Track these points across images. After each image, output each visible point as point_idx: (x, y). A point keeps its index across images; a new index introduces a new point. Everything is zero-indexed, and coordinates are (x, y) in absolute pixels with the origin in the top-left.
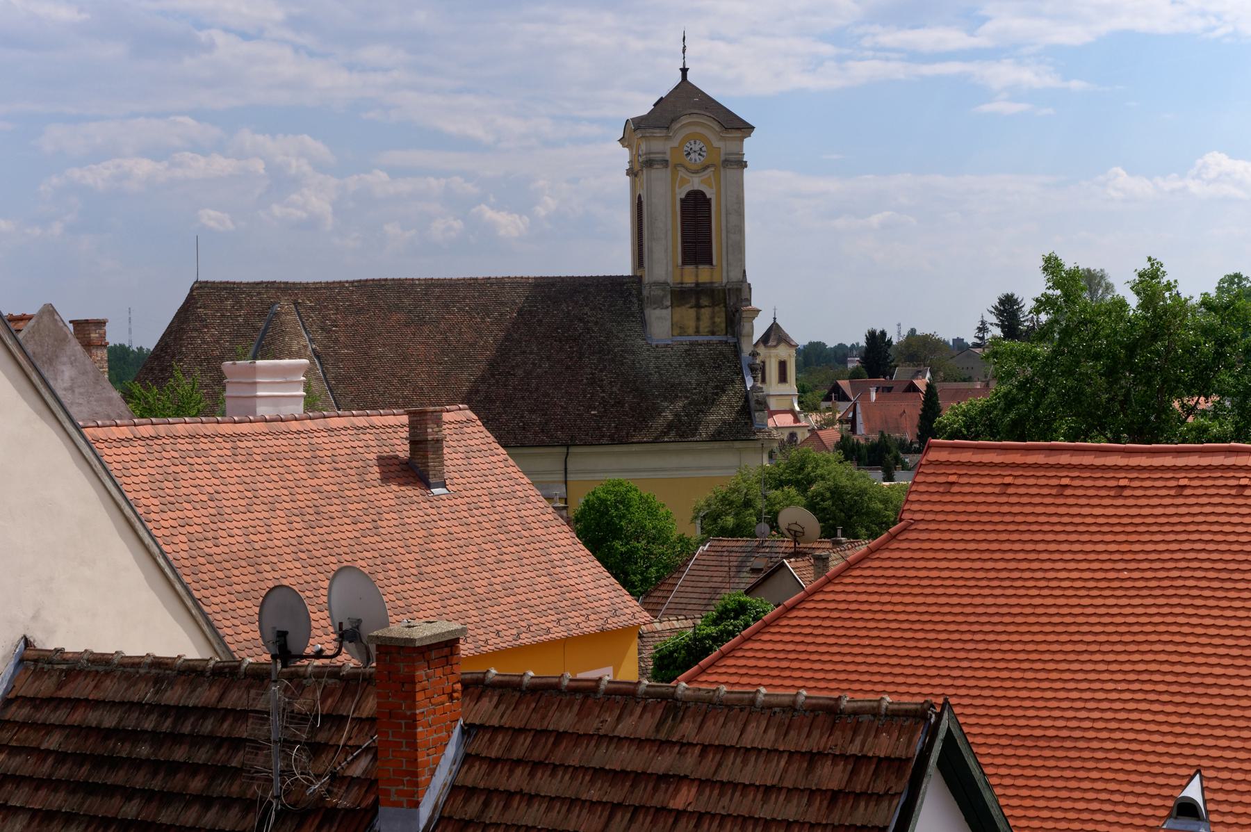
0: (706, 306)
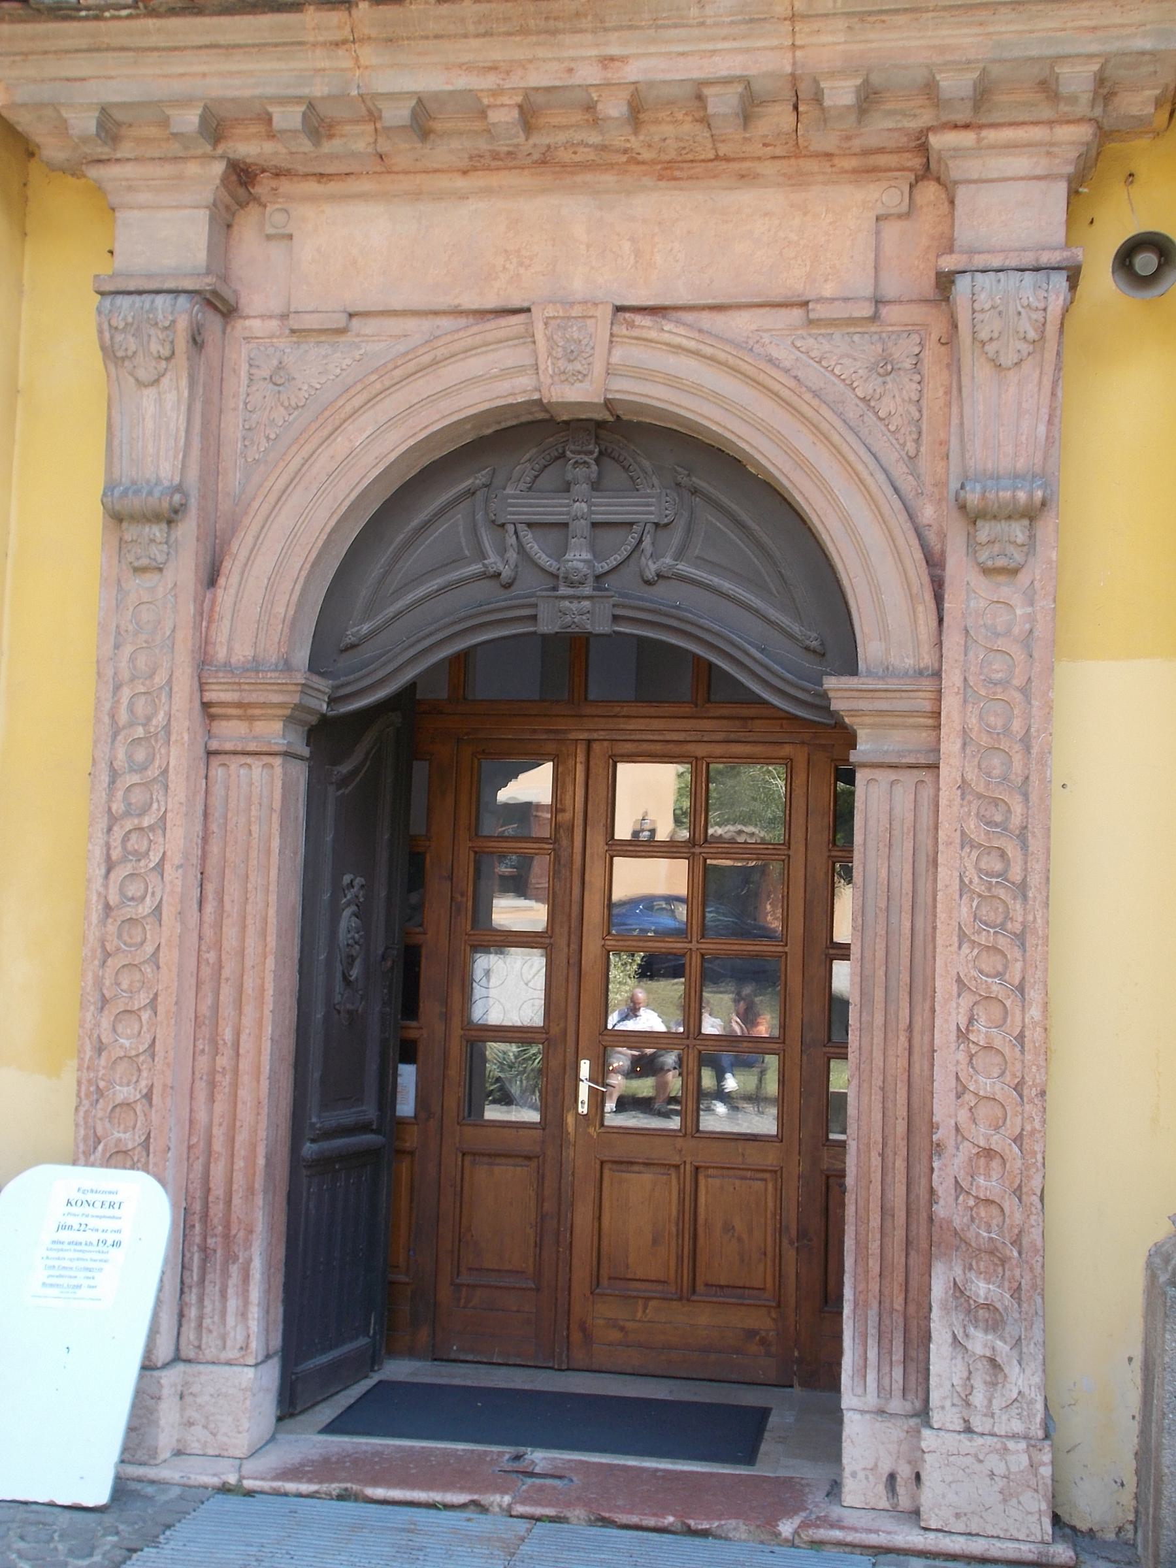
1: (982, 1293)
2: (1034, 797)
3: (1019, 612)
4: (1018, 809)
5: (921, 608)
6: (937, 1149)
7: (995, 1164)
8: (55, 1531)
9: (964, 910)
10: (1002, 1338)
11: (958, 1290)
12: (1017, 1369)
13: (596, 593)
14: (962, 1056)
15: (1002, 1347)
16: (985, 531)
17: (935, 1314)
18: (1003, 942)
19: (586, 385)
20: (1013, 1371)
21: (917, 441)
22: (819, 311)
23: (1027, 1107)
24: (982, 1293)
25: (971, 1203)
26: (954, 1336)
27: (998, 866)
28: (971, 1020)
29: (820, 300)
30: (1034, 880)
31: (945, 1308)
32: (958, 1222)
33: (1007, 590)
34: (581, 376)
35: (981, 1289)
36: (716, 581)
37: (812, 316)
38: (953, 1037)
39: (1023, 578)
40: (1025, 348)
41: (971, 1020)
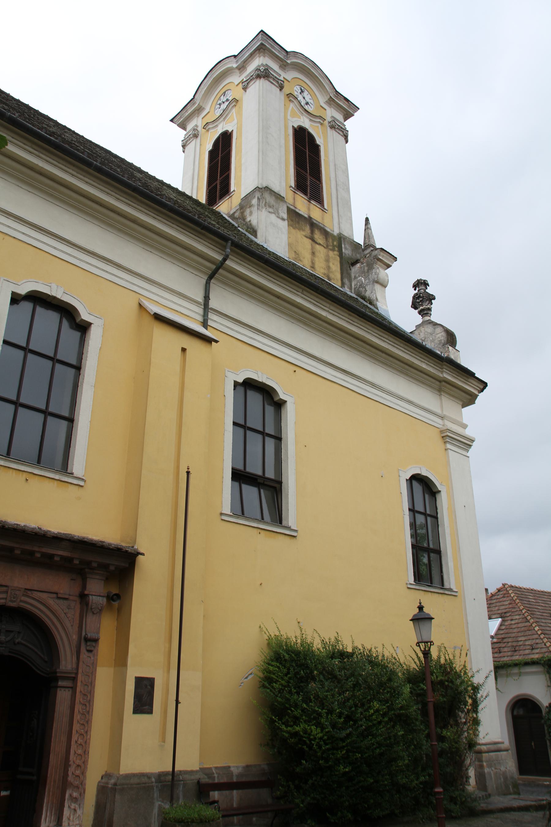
0: (320, 244)
1: (75, 795)
2: (92, 694)
3: (92, 658)
4: (89, 697)
5: (74, 656)
6: (70, 765)
7: (79, 768)
8: (401, 704)
9: (79, 717)
10: (77, 805)
11: (71, 795)
12: (79, 810)
13: (431, 707)
14: (76, 746)
15: (77, 806)
16: (89, 643)
17: (66, 801)
18: (84, 723)
19: (15, 603)
20: (78, 811)
21: (73, 622)
22: (60, 596)
23: (86, 756)
24: (75, 795)
25: (74, 776)
26: (69, 806)
27: (85, 708)
28: (78, 739)
29: (60, 593)
30: (91, 711)
31: (68, 800)
32: (72, 781)
33: (90, 654)
34: (14, 601)
35: (75, 794)
36: (29, 645)
37: (58, 596)
38: (75, 742)
39: (93, 652)
40: (98, 610)
41: (78, 739)
